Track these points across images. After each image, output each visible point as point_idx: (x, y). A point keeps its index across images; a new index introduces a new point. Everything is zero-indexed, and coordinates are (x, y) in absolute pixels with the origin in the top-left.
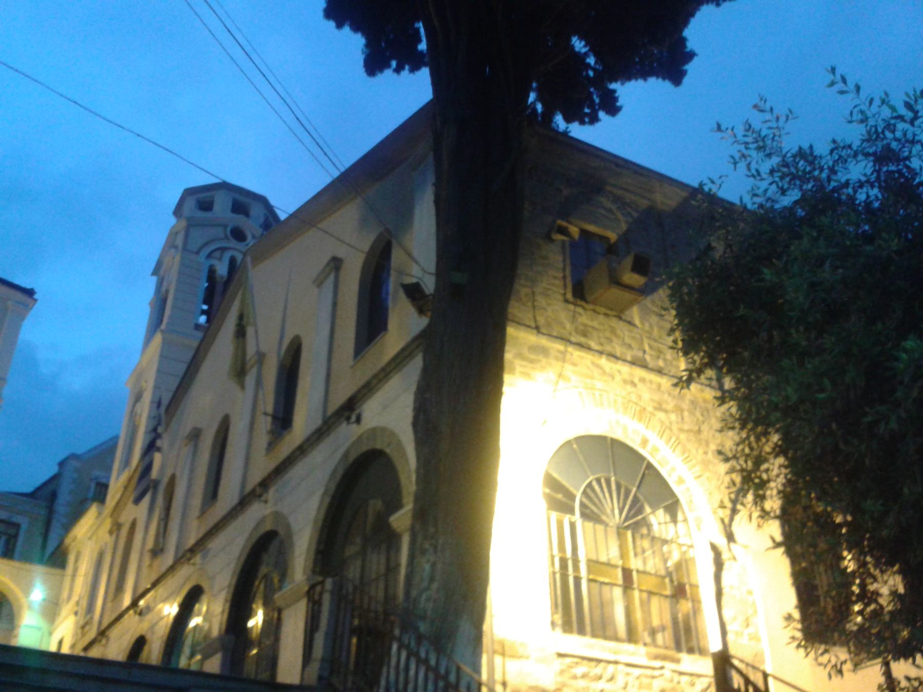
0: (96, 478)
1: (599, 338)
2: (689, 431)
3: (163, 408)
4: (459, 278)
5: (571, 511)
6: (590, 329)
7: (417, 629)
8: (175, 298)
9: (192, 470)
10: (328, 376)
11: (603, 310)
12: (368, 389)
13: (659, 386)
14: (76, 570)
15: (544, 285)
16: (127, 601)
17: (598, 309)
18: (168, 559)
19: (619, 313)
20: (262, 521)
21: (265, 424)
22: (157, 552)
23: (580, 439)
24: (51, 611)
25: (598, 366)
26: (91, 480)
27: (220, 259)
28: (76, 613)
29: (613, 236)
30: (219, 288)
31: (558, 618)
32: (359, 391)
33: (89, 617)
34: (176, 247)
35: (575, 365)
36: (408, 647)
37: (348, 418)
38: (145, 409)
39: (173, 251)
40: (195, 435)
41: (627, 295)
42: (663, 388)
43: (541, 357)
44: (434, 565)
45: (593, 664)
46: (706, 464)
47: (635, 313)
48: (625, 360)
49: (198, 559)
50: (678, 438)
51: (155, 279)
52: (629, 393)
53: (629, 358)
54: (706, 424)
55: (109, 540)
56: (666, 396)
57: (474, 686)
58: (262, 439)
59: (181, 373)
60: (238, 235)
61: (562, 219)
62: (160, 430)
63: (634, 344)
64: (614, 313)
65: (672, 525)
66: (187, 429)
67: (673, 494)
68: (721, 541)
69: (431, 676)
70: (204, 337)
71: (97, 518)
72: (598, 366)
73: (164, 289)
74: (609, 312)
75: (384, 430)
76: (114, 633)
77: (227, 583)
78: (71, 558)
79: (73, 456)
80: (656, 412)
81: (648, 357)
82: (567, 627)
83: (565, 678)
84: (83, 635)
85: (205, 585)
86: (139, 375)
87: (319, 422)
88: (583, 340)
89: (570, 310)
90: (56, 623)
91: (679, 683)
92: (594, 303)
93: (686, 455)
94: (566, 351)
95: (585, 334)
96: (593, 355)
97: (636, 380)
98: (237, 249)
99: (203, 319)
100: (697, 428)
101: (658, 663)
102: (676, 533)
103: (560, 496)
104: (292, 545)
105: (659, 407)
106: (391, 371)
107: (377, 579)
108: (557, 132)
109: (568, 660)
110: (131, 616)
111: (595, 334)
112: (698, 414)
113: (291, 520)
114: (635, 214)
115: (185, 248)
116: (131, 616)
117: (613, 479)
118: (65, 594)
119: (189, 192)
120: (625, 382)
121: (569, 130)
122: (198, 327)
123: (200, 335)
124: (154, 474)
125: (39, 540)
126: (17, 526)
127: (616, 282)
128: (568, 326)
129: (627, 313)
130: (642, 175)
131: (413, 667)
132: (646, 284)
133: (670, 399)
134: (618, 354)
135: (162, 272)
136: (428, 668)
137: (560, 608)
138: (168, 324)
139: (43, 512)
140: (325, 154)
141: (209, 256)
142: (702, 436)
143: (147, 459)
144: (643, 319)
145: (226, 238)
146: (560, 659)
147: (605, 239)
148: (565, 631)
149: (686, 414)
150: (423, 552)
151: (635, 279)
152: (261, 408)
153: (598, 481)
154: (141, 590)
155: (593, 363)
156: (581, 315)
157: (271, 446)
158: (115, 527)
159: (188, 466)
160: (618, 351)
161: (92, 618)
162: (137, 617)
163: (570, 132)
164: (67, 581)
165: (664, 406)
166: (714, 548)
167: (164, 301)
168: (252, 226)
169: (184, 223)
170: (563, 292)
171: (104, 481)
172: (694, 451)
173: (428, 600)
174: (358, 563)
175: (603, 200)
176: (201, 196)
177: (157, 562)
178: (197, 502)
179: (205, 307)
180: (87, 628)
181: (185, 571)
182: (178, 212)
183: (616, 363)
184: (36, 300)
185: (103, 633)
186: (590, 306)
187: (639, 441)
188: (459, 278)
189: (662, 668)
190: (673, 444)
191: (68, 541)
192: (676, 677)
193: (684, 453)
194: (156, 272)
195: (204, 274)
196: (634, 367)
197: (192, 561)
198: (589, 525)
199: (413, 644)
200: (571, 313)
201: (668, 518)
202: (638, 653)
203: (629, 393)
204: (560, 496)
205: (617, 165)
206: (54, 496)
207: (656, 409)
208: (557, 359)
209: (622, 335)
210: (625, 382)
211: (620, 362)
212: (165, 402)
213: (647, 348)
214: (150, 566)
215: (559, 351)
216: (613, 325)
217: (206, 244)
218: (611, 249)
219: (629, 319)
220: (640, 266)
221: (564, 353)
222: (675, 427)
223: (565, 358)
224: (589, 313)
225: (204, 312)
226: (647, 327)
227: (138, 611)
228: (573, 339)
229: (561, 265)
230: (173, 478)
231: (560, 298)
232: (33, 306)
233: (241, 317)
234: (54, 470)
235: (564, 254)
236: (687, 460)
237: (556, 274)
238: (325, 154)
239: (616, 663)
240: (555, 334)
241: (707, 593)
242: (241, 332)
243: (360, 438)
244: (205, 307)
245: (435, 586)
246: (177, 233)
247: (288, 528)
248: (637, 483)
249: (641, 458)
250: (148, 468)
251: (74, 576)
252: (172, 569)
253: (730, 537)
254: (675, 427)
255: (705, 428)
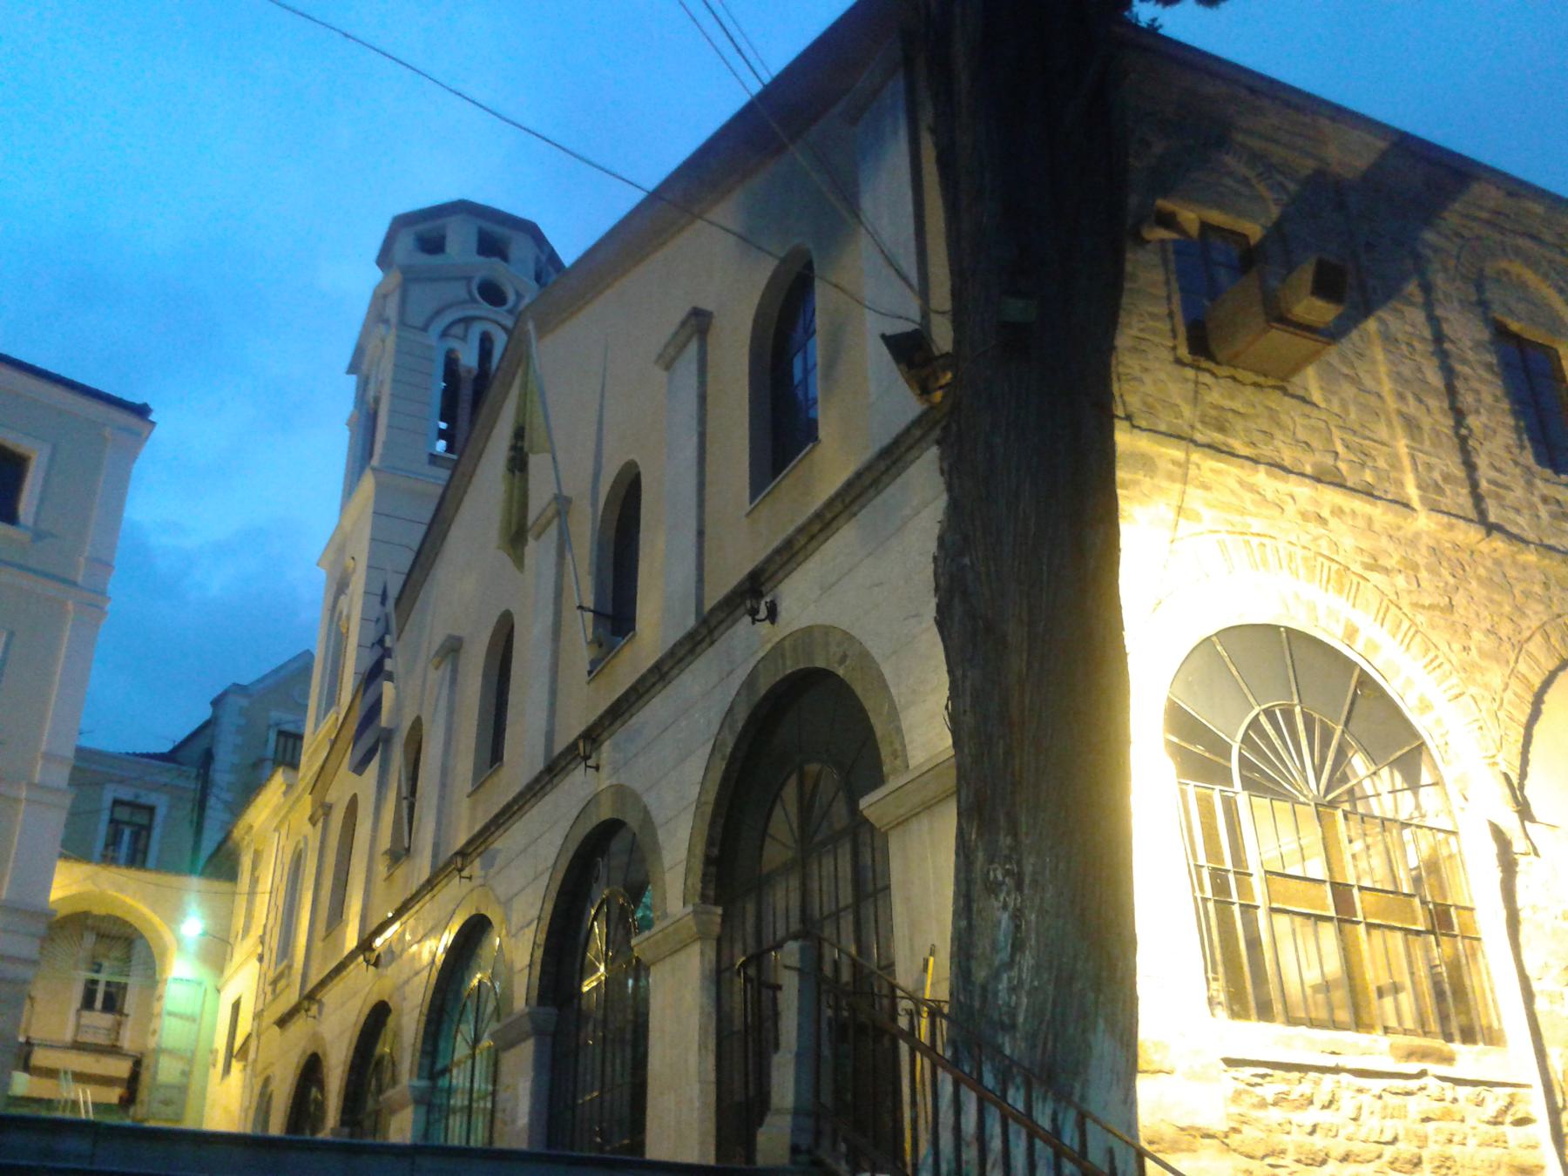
0: (277, 724)
1: (1247, 431)
2: (1432, 607)
3: (391, 602)
4: (1016, 309)
5: (1228, 780)
6: (1230, 415)
7: (999, 1050)
8: (393, 412)
9: (451, 711)
10: (701, 533)
11: (1250, 377)
12: (788, 555)
13: (1370, 521)
14: (255, 881)
15: (1134, 332)
16: (351, 941)
17: (1241, 374)
18: (422, 867)
19: (1279, 377)
20: (593, 802)
21: (580, 629)
22: (399, 854)
23: (1232, 634)
24: (217, 952)
25: (1252, 489)
26: (269, 727)
27: (464, 338)
28: (261, 958)
29: (1254, 231)
30: (466, 392)
31: (1219, 989)
32: (769, 560)
33: (285, 963)
34: (386, 321)
35: (1206, 487)
36: (977, 1085)
37: (753, 612)
38: (355, 604)
39: (382, 328)
40: (452, 649)
41: (1305, 344)
42: (1377, 527)
43: (1140, 476)
44: (1017, 916)
45: (1296, 1075)
46: (1467, 669)
47: (1310, 380)
48: (1302, 475)
49: (475, 867)
50: (1413, 623)
51: (353, 379)
52: (1316, 539)
53: (1308, 469)
54: (1461, 591)
55: (313, 835)
56: (1384, 541)
57: (1124, 1162)
58: (580, 651)
59: (415, 545)
60: (492, 293)
61: (1165, 196)
62: (388, 641)
63: (1315, 444)
64: (1271, 382)
65: (1408, 793)
66: (436, 638)
67: (1413, 733)
68: (1510, 823)
69: (1043, 1151)
70: (452, 477)
71: (285, 793)
72: (1252, 489)
73: (371, 394)
74: (1261, 380)
75: (827, 630)
76: (331, 996)
77: (535, 912)
78: (246, 862)
79: (238, 689)
80: (1368, 574)
81: (1342, 466)
82: (1237, 1006)
83: (1244, 1107)
84: (276, 995)
85: (494, 915)
86: (338, 547)
87: (691, 622)
88: (1218, 437)
89: (1186, 380)
90: (228, 972)
91: (1455, 1100)
92: (1231, 363)
93: (1431, 655)
94: (1188, 461)
95: (1221, 429)
96: (1242, 467)
97: (1325, 513)
98: (494, 322)
99: (441, 445)
100: (1445, 601)
101: (1413, 1067)
102: (1418, 807)
103: (1199, 749)
104: (656, 848)
105: (1374, 566)
106: (835, 518)
107: (836, 916)
108: (1136, 27)
109: (1246, 1073)
110: (359, 972)
111: (1239, 425)
112: (1445, 573)
113: (650, 800)
114: (1292, 187)
115: (403, 323)
116: (359, 972)
117: (1298, 709)
118: (239, 922)
119: (402, 223)
120: (1304, 515)
121: (1157, 24)
122: (434, 459)
123: (444, 474)
124: (385, 719)
125: (187, 834)
126: (151, 810)
127: (1280, 318)
128: (1187, 411)
129: (1296, 379)
130: (1297, 109)
131: (994, 1128)
132: (1339, 317)
133: (1391, 547)
134: (1287, 463)
135: (364, 367)
136: (1033, 1133)
137: (1220, 969)
138: (383, 457)
139: (192, 785)
140: (739, 50)
141: (445, 334)
142: (1456, 617)
143: (370, 697)
144: (1327, 391)
145: (473, 300)
146: (1233, 1071)
147: (1241, 237)
148: (1234, 1015)
149: (1423, 574)
150: (993, 888)
151: (1320, 311)
152: (571, 600)
153: (1269, 713)
154: (374, 923)
155: (1241, 483)
156: (1209, 387)
157: (596, 669)
158: (320, 812)
159: (443, 703)
160: (1287, 457)
161: (290, 967)
162: (371, 968)
163: (1161, 26)
164: (241, 903)
165: (1382, 562)
166: (1498, 834)
167: (373, 417)
168: (516, 276)
169: (396, 277)
170: (1170, 344)
171: (289, 728)
172: (1444, 647)
173: (1013, 989)
174: (794, 882)
175: (1229, 159)
176: (422, 227)
177: (400, 872)
178: (465, 765)
179: (443, 425)
180: (282, 983)
181: (453, 888)
182: (384, 259)
183: (1287, 482)
184: (153, 424)
185: (310, 997)
186: (1224, 371)
187: (1340, 632)
188: (1016, 309)
189: (1423, 1074)
190: (1406, 634)
191: (237, 833)
192: (1450, 1090)
193: (1427, 650)
194: (353, 368)
195: (439, 370)
196: (1319, 486)
197: (465, 873)
198: (1262, 803)
199: (989, 1080)
200: (1191, 386)
201: (1399, 782)
202: (1373, 1049)
203: (1316, 539)
204: (1199, 749)
205: (1252, 90)
206: (208, 757)
207: (1368, 567)
208: (1171, 477)
209: (1289, 422)
210: (1304, 515)
211: (1292, 477)
212: (393, 593)
213: (1340, 448)
214: (389, 878)
215: (1174, 462)
216: (1273, 406)
217: (438, 313)
218: (1249, 258)
219: (1301, 393)
220: (1328, 285)
221: (1184, 466)
222: (1404, 602)
223: (1186, 475)
224: (1222, 381)
225: (442, 434)
226: (1336, 408)
227: (373, 957)
228: (1198, 437)
229: (1162, 292)
230: (417, 724)
231: (1167, 356)
232: (150, 433)
233: (519, 434)
234: (206, 713)
235: (1167, 270)
236: (1433, 664)
237: (1155, 310)
238: (739, 50)
239: (1336, 1070)
240: (1163, 428)
241: (1489, 920)
242: (518, 463)
243: (778, 648)
244: (443, 425)
245: (1028, 960)
246: (385, 296)
247: (647, 820)
248: (1343, 718)
249: (1349, 664)
250: (374, 711)
251: (252, 893)
252: (430, 885)
253: (1524, 811)
254: (1404, 602)
255: (1460, 599)
